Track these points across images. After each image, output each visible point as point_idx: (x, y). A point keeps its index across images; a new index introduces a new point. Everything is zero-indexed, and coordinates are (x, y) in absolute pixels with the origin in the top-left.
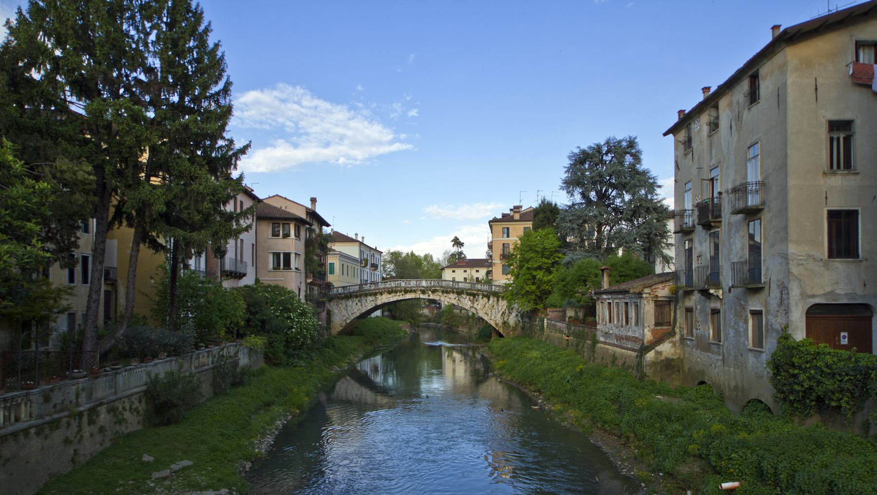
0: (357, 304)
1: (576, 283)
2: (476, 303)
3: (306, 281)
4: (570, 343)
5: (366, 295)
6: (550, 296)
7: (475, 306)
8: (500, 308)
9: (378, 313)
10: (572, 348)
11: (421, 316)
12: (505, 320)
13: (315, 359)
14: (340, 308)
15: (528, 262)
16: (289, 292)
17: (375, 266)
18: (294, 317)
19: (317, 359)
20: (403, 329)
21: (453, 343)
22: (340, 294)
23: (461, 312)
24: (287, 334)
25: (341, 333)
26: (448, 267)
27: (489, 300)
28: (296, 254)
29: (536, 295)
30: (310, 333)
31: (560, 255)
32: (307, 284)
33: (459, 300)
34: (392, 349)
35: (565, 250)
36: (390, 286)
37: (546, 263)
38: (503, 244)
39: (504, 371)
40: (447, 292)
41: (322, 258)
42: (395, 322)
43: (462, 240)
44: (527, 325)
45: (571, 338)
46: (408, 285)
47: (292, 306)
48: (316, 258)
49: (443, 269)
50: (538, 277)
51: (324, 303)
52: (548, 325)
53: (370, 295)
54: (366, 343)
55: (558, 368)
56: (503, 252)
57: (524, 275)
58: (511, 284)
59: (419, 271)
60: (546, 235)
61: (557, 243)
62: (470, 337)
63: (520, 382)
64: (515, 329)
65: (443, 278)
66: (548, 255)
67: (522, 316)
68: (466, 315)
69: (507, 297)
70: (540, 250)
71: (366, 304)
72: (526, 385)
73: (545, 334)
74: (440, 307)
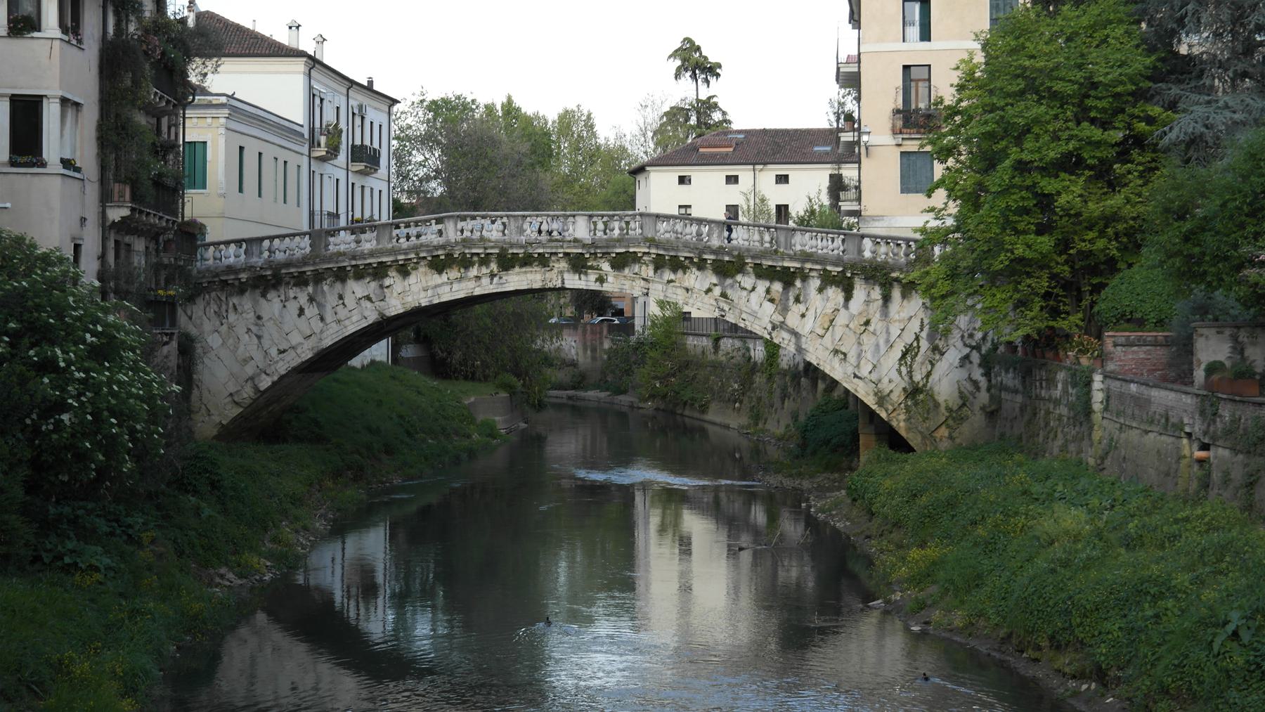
0: (301, 312)
1: (1242, 226)
2: (796, 309)
3: (103, 215)
4: (1216, 476)
5: (341, 275)
6: (1115, 281)
7: (793, 320)
8: (895, 331)
9: (379, 351)
10: (1227, 494)
11: (547, 361)
12: (918, 377)
13: (146, 537)
14: (231, 327)
15: (1019, 141)
16: (46, 260)
17: (366, 157)
18: (69, 363)
19: (153, 542)
20: (480, 418)
21: (679, 472)
22: (230, 269)
23: (716, 347)
24: (36, 430)
25: (234, 433)
26: (658, 163)
27: (848, 298)
28: (64, 101)
29: (1053, 277)
30: (132, 432)
31: (1154, 110)
32: (107, 228)
33: (724, 295)
34: (433, 499)
35: (1175, 90)
36: (441, 240)
37: (1098, 144)
38: (906, 68)
39: (934, 589)
40: (677, 265)
41: (165, 121)
42: (450, 389)
43: (712, 53)
44: (1013, 402)
45: (1220, 454)
46: (515, 238)
47: (60, 317)
48: (141, 119)
49: (641, 170)
50: (1062, 200)
51: (171, 304)
52: (1108, 398)
53: (359, 274)
54: (337, 474)
55: (1182, 579)
56: (906, 100)
57: (1006, 191)
58: (948, 231)
59: (546, 179)
60: (1093, 27)
61: (1142, 62)
62: (757, 452)
63: (1010, 636)
64: (956, 416)
65: (640, 206)
66: (1104, 110)
67: (987, 364)
68: (738, 358)
69: (932, 286)
70: (1069, 89)
71: (342, 313)
72: (1039, 648)
73: (1097, 435)
74: (627, 327)
